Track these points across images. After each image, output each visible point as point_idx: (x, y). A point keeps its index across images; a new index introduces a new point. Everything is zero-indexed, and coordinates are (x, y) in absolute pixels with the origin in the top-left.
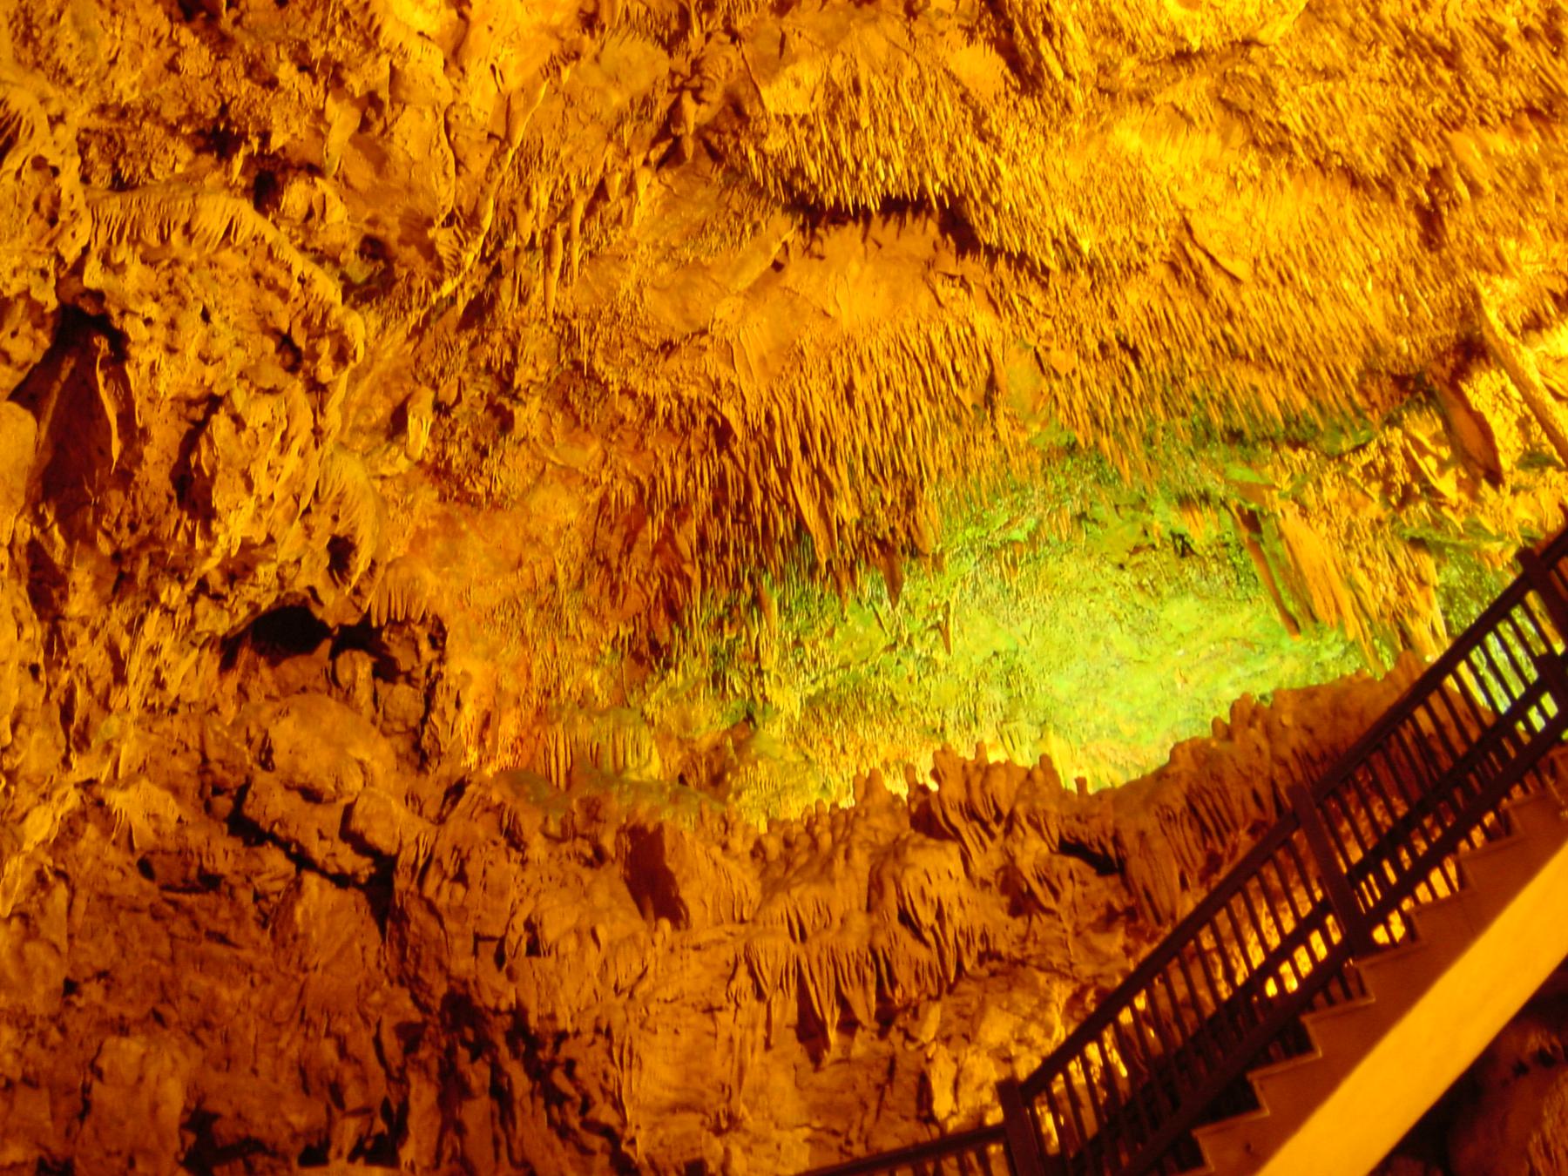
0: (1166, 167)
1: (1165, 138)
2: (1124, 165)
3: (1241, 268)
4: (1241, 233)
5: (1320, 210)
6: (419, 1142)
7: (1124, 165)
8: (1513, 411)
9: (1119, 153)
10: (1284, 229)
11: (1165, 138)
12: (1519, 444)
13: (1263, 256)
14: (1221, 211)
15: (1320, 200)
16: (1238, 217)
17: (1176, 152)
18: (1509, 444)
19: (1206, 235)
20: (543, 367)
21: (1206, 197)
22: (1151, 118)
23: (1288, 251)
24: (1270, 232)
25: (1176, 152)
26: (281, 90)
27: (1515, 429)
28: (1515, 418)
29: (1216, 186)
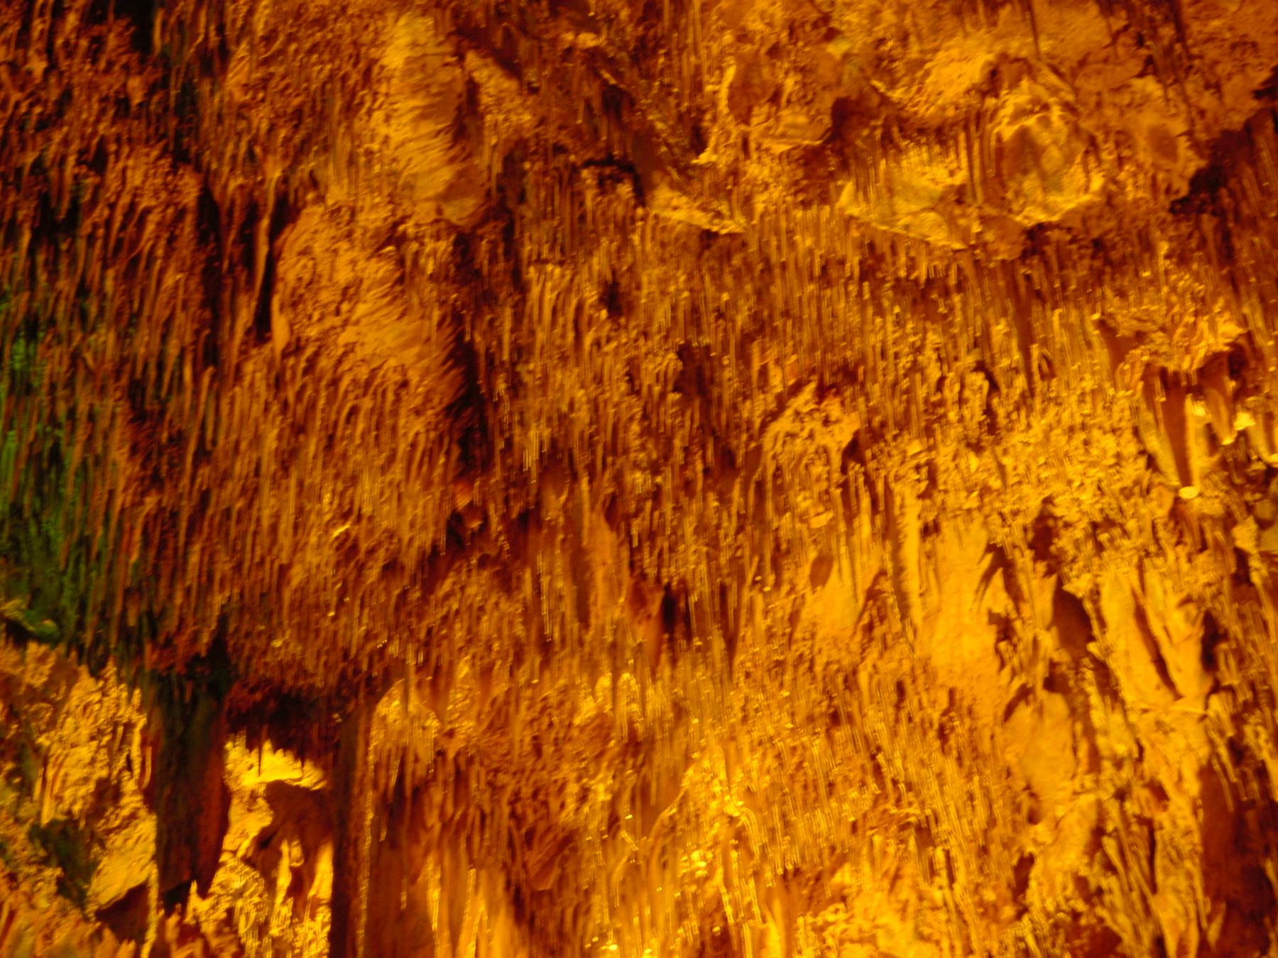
0: (383, 130)
1: (419, 102)
2: (362, 65)
3: (280, 332)
4: (325, 296)
5: (405, 384)
6: (127, 564)
7: (362, 65)
8: (110, 765)
9: (374, 43)
10: (360, 353)
11: (419, 102)
12: (77, 808)
13: (309, 351)
14: (344, 245)
15: (414, 377)
16: (344, 275)
17: (406, 132)
18: (68, 794)
19: (298, 246)
20: (893, 464)
21: (353, 213)
22: (436, 62)
23: (335, 382)
24: (347, 336)
25: (406, 132)
26: (1100, 557)
27: (91, 787)
28: (104, 773)
29: (374, 217)
